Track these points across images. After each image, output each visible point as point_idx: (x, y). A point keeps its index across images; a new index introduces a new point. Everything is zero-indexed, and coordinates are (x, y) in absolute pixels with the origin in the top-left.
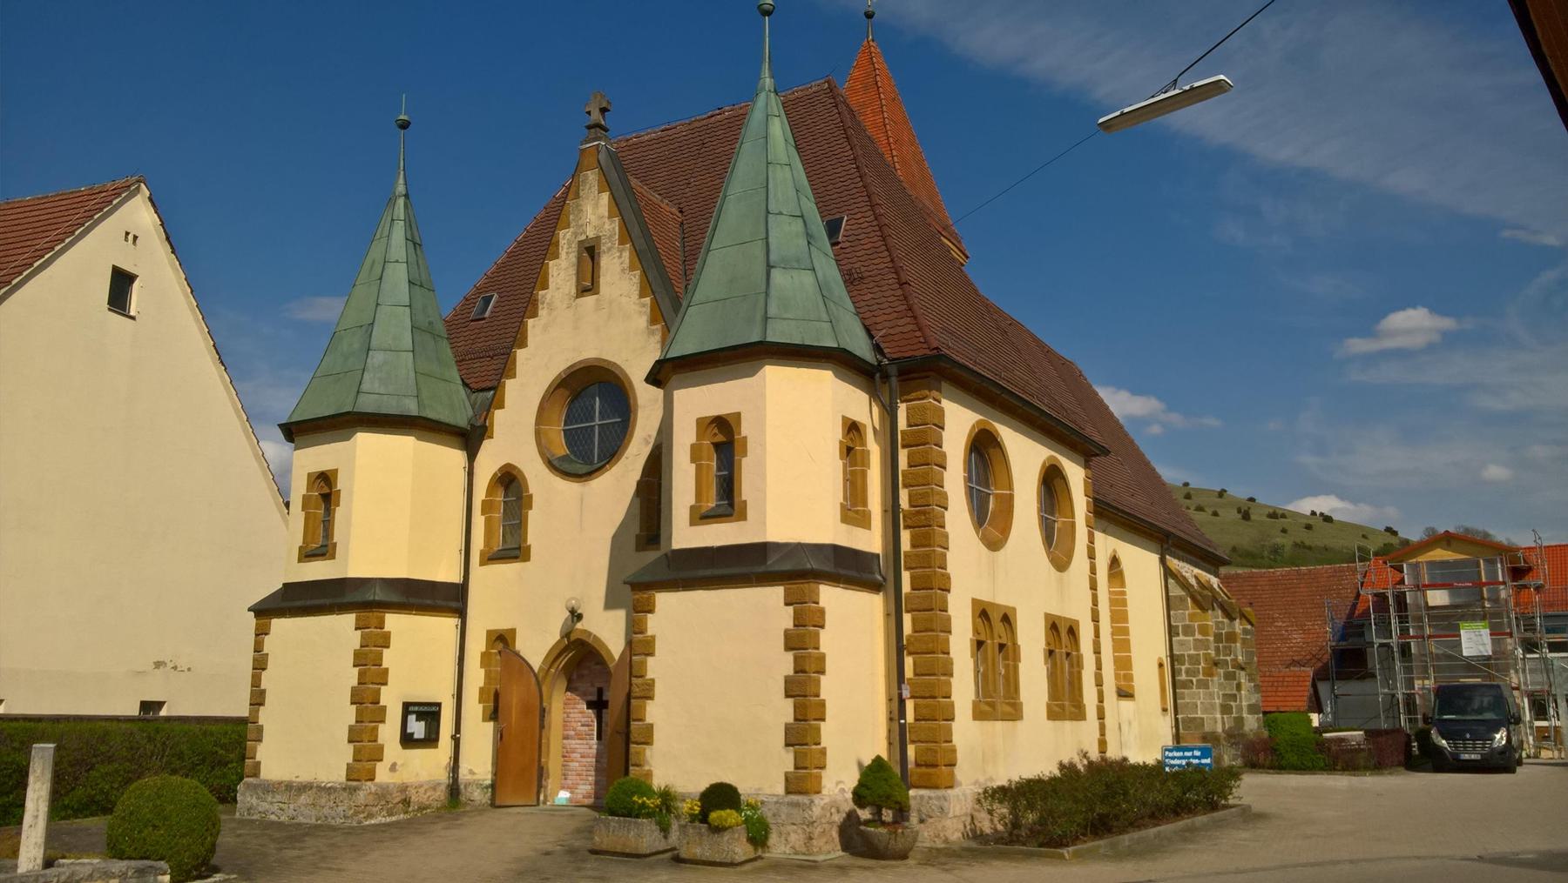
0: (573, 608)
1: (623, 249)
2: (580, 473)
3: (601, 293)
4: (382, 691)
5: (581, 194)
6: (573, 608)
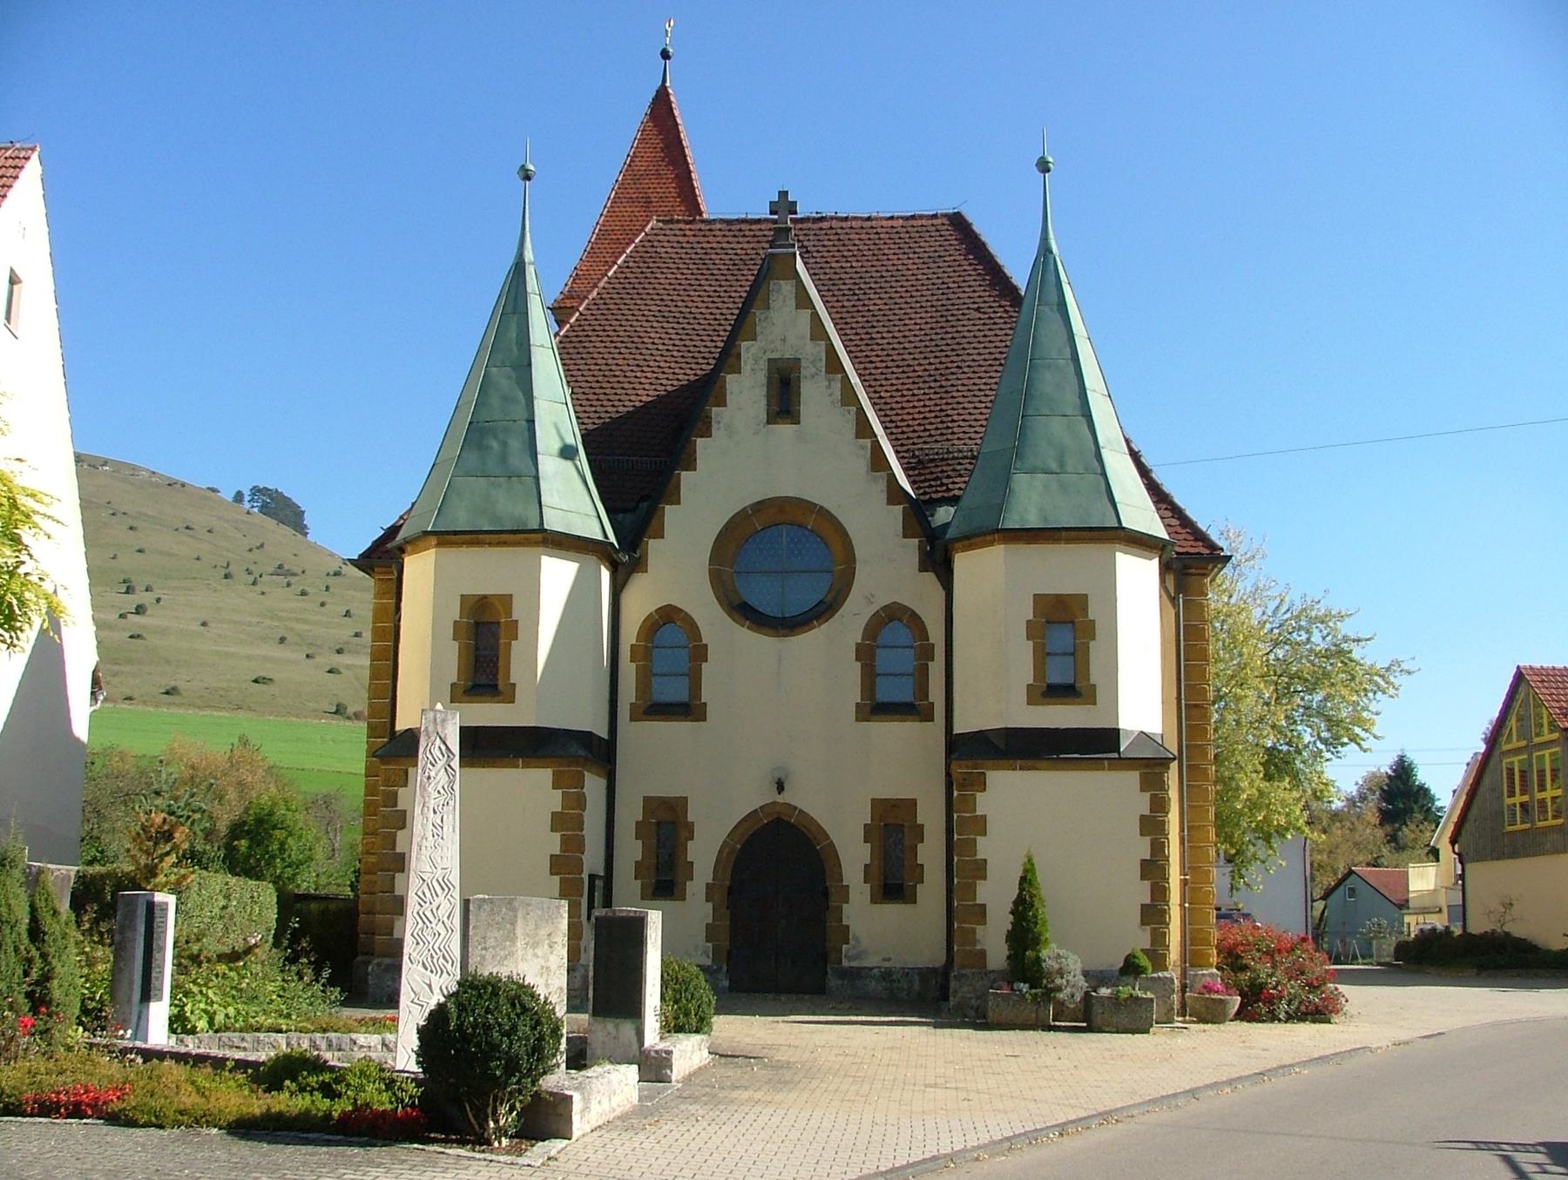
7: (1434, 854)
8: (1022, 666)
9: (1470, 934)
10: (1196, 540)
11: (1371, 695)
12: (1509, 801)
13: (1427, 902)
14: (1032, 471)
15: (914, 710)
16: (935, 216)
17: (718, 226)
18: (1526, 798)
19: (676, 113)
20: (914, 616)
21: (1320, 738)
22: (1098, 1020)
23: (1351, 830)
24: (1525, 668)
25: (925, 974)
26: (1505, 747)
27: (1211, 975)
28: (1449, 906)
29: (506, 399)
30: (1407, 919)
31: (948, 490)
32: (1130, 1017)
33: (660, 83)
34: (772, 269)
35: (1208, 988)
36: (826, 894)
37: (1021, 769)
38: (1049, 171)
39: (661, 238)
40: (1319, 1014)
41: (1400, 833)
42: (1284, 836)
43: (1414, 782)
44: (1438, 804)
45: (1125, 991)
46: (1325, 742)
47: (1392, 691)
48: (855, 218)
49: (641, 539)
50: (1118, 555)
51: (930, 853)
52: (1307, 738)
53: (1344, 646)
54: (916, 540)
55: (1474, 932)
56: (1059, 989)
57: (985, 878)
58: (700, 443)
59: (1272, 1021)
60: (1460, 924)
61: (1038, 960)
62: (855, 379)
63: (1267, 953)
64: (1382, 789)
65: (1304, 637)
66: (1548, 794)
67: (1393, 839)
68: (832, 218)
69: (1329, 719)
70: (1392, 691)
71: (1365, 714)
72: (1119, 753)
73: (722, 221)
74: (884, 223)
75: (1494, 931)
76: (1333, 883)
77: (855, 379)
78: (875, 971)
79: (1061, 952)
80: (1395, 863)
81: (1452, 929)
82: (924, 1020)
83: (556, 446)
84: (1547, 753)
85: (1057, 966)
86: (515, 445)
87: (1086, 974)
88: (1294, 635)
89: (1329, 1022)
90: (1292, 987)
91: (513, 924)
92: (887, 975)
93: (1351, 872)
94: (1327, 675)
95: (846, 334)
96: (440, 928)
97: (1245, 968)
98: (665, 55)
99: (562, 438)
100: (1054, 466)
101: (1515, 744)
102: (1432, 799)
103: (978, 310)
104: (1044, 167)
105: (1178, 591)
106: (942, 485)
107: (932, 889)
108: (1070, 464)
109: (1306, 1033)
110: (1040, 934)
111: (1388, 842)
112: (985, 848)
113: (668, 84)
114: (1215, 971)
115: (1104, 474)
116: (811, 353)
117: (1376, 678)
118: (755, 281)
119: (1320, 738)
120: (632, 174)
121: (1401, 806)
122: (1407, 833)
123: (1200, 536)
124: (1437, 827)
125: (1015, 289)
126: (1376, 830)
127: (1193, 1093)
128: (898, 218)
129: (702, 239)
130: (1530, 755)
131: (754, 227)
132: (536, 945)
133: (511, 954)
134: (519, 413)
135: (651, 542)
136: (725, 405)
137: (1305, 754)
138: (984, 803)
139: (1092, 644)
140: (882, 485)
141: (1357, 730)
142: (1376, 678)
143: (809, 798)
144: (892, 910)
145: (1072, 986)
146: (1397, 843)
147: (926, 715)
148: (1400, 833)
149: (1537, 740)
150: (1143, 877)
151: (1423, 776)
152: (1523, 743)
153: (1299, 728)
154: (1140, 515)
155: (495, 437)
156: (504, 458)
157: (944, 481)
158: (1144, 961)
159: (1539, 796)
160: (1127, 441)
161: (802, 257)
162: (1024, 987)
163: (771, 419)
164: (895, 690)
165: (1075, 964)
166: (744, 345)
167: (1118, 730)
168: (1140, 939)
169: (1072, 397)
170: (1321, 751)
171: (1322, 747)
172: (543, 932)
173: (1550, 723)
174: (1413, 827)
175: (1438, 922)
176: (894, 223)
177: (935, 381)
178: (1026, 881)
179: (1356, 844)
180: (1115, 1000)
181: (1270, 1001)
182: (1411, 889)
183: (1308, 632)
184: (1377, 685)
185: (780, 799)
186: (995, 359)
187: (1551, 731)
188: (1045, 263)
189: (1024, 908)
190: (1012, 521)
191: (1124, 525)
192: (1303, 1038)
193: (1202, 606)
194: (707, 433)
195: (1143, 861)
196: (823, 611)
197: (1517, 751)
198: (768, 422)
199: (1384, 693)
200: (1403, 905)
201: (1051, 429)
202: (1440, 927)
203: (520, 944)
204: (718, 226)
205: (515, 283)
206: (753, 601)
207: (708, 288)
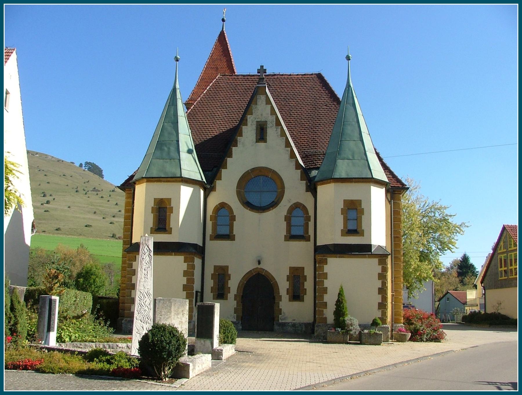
0: (259, 260)
1: (278, 128)
2: (263, 205)
3: (267, 142)
4: (381, 315)
5: (258, 104)
6: (259, 260)
7: (475, 287)
8: (340, 224)
9: (487, 313)
10: (397, 182)
11: (455, 234)
12: (500, 269)
13: (473, 303)
15: (304, 237)
16: (312, 74)
17: (240, 77)
18: (506, 268)
23: (448, 278)
24: (506, 225)
25: (307, 325)
26: (499, 252)
27: (401, 326)
28: (480, 304)
29: (170, 134)
30: (466, 308)
31: (316, 165)
32: (374, 340)
35: (400, 331)
36: (274, 298)
38: (350, 60)
39: (221, 81)
40: (437, 339)
41: (464, 280)
43: (469, 263)
44: (477, 270)
45: (373, 331)
46: (439, 249)
47: (462, 233)
51: (309, 285)
52: (434, 248)
55: (488, 313)
56: (351, 330)
58: (234, 148)
60: (484, 310)
61: (344, 321)
62: (285, 128)
64: (458, 265)
65: (433, 214)
67: (462, 281)
69: (441, 242)
70: (462, 233)
71: (453, 240)
72: (371, 252)
74: (295, 76)
75: (495, 312)
76: (442, 296)
77: (285, 128)
80: (462, 289)
81: (481, 311)
83: (186, 149)
85: (350, 323)
86: (173, 149)
87: (360, 325)
88: (430, 214)
90: (428, 330)
91: (171, 307)
92: (294, 325)
93: (448, 292)
94: (440, 227)
95: (282, 113)
96: (146, 308)
97: (412, 324)
98: (223, 20)
100: (351, 157)
101: (502, 250)
102: (475, 269)
103: (326, 105)
104: (348, 58)
106: (314, 163)
107: (309, 297)
111: (460, 283)
112: (327, 283)
113: (224, 30)
114: (403, 325)
115: (367, 160)
116: (271, 119)
117: (457, 228)
119: (438, 248)
120: (212, 59)
121: (465, 271)
122: (466, 280)
123: (399, 181)
125: (338, 99)
127: (395, 365)
128: (300, 75)
131: (252, 77)
132: (178, 314)
133: (170, 317)
138: (327, 269)
139: (363, 216)
142: (457, 228)
143: (268, 267)
145: (355, 329)
148: (464, 280)
149: (510, 249)
150: (379, 294)
152: (505, 250)
153: (431, 245)
154: (379, 174)
155: (166, 146)
156: (169, 153)
157: (314, 162)
158: (379, 321)
160: (375, 149)
161: (268, 88)
162: (339, 330)
164: (299, 232)
167: (371, 245)
168: (378, 314)
169: (357, 134)
171: (438, 251)
174: (468, 278)
175: (477, 309)
176: (299, 77)
177: (312, 129)
178: (340, 294)
179: (450, 283)
180: (369, 334)
181: (421, 335)
182: (467, 298)
183: (434, 213)
185: (259, 267)
186: (332, 122)
188: (348, 90)
189: (339, 303)
190: (337, 175)
191: (374, 177)
193: (399, 204)
194: (236, 145)
196: (274, 204)
199: (459, 233)
200: (465, 303)
201: (350, 145)
203: (173, 314)
204: (240, 77)
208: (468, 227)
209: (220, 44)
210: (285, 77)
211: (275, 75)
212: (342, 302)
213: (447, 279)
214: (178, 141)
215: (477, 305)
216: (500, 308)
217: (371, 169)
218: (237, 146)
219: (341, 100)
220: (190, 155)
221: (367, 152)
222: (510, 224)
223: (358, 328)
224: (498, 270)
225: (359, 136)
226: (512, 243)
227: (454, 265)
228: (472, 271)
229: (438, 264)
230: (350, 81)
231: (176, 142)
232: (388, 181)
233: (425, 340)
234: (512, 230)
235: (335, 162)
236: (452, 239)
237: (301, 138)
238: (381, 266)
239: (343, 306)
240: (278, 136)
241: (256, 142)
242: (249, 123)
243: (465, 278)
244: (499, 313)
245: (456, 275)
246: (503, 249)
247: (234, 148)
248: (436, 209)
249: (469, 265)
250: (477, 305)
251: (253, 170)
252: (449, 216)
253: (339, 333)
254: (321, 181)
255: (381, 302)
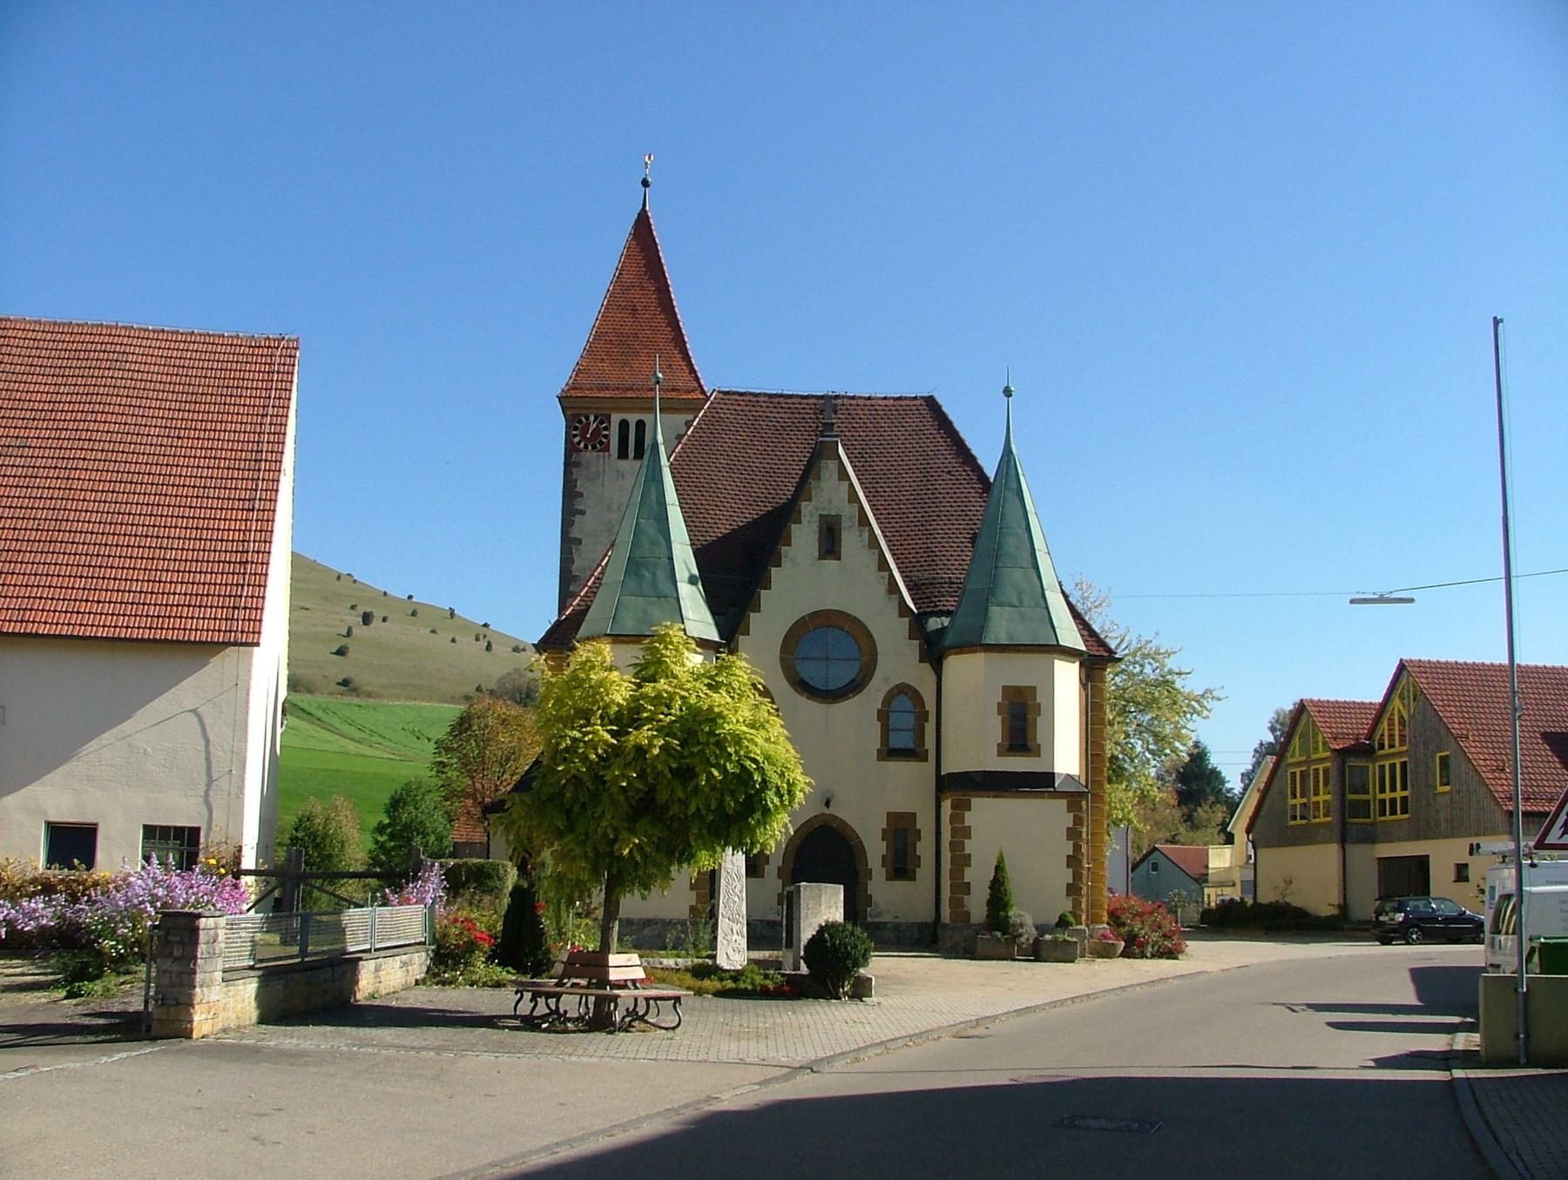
2: (834, 685)
7: (1230, 839)
8: (994, 730)
9: (1260, 904)
10: (1099, 646)
11: (1188, 716)
12: (1292, 802)
13: (1223, 878)
14: (1001, 605)
15: (913, 753)
16: (915, 398)
17: (763, 399)
18: (1304, 800)
19: (655, 233)
20: (916, 692)
21: (1148, 749)
22: (1044, 954)
23: (1152, 810)
24: (1307, 701)
25: (922, 926)
26: (1291, 760)
27: (1104, 928)
28: (1242, 882)
29: (654, 543)
30: (1206, 891)
31: (936, 606)
32: (1065, 954)
33: (641, 207)
34: (820, 453)
35: (1105, 937)
36: (856, 873)
37: (995, 797)
38: (1011, 395)
39: (723, 406)
40: (1171, 954)
41: (1195, 814)
42: (1118, 826)
43: (1207, 766)
44: (1228, 786)
45: (1061, 937)
46: (1152, 752)
47: (1205, 713)
48: (860, 398)
49: (733, 636)
50: (1056, 662)
51: (925, 848)
52: (1139, 749)
53: (1169, 677)
54: (918, 642)
55: (1263, 902)
56: (1021, 935)
57: (970, 866)
58: (774, 570)
59: (1142, 958)
60: (1251, 896)
61: (1007, 917)
62: (878, 531)
63: (1136, 915)
64: (1178, 772)
65: (1138, 669)
66: (1322, 798)
67: (1188, 818)
68: (843, 397)
69: (1155, 735)
70: (1205, 713)
71: (1184, 731)
72: (1054, 787)
73: (765, 395)
74: (880, 402)
75: (1277, 901)
76: (1138, 859)
77: (878, 531)
78: (889, 925)
79: (1021, 913)
80: (1190, 840)
81: (1246, 900)
82: (108, 1037)
83: (687, 576)
84: (1321, 767)
85: (1019, 921)
86: (661, 575)
87: (1037, 927)
88: (1131, 667)
89: (1177, 958)
90: (1155, 937)
91: (820, 896)
92: (896, 927)
93: (1155, 849)
94: (1155, 700)
95: (878, 509)
96: (736, 899)
97: (1124, 924)
98: (645, 183)
99: (689, 570)
100: (1016, 603)
101: (1297, 759)
102: (1223, 782)
103: (949, 472)
104: (1008, 393)
105: (1087, 681)
106: (931, 602)
107: (925, 872)
108: (1025, 602)
109: (1165, 964)
110: (1008, 901)
111: (1185, 821)
112: (970, 846)
113: (647, 208)
114: (1106, 926)
115: (1047, 608)
116: (848, 511)
117: (1193, 703)
118: (811, 457)
119: (1148, 749)
120: (620, 285)
121: (1195, 787)
122: (1201, 812)
123: (1102, 643)
124: (1232, 817)
125: (987, 478)
126: (1174, 811)
127: (1123, 988)
128: (891, 398)
129: (752, 409)
130: (1309, 768)
131: (789, 401)
132: (830, 907)
133: (820, 912)
134: (662, 551)
135: (741, 637)
136: (790, 545)
137: (1136, 761)
138: (970, 818)
139: (1038, 719)
140: (896, 604)
141: (1177, 744)
142: (1193, 703)
143: (845, 812)
144: (900, 885)
145: (1029, 933)
146: (1193, 823)
147: (923, 758)
148: (1195, 814)
149: (1314, 756)
150: (1068, 866)
151: (1215, 760)
152: (1304, 758)
153: (1132, 741)
154: (1070, 636)
155: (647, 569)
156: (654, 584)
157: (934, 599)
158: (1071, 919)
159: (1314, 799)
160: (1060, 583)
161: (842, 445)
162: (999, 934)
163: (822, 557)
164: (901, 740)
165: (1029, 921)
166: (804, 504)
167: (1054, 774)
168: (1066, 905)
169: (1027, 556)
170: (1148, 760)
171: (1149, 756)
172: (833, 901)
173: (1324, 744)
174: (1206, 807)
175: (1234, 894)
176: (887, 402)
177: (922, 525)
178: (999, 868)
179: (1156, 823)
180: (1055, 942)
181: (1142, 945)
182: (1210, 866)
183: (1142, 666)
184: (1194, 708)
185: (827, 811)
186: (962, 511)
187: (1324, 751)
188: (1009, 461)
189: (998, 885)
190: (990, 639)
191: (1061, 643)
192: (1164, 966)
193: (1102, 689)
194: (779, 565)
195: (1068, 857)
196: (855, 687)
197: (1298, 764)
198: (820, 558)
199: (1199, 715)
200: (1202, 879)
201: (1014, 576)
202: (1238, 899)
203: (823, 907)
204: (763, 399)
205: (651, 464)
206: (806, 676)
207: (760, 448)
208: (1219, 699)
209: (637, 244)
210: (860, 402)
211: (837, 397)
212: (1003, 884)
213: (1149, 812)
214: (671, 559)
215: (1234, 885)
216: (1288, 891)
217: (1055, 625)
218: (780, 566)
219: (992, 480)
220: (694, 588)
221: (1046, 592)
222: (1315, 698)
223: (1035, 932)
224: (1286, 803)
225: (1030, 558)
226: (1321, 744)
227: (1167, 771)
228: (1214, 788)
229: (1148, 787)
230: (1012, 439)
231: (666, 560)
232: (1084, 649)
233: (1148, 955)
234: (1320, 712)
235: (986, 609)
236: (1183, 727)
237: (901, 545)
238: (1072, 815)
239: (1005, 890)
240: (863, 546)
241: (820, 558)
242: (804, 520)
243: (1199, 809)
244: (1287, 903)
245: (1174, 802)
246: (1300, 755)
247: (774, 570)
248: (1145, 656)
249: (1208, 772)
250: (1234, 885)
251: (815, 615)
252: (1177, 674)
253: (999, 940)
254: (953, 647)
255: (1071, 881)
